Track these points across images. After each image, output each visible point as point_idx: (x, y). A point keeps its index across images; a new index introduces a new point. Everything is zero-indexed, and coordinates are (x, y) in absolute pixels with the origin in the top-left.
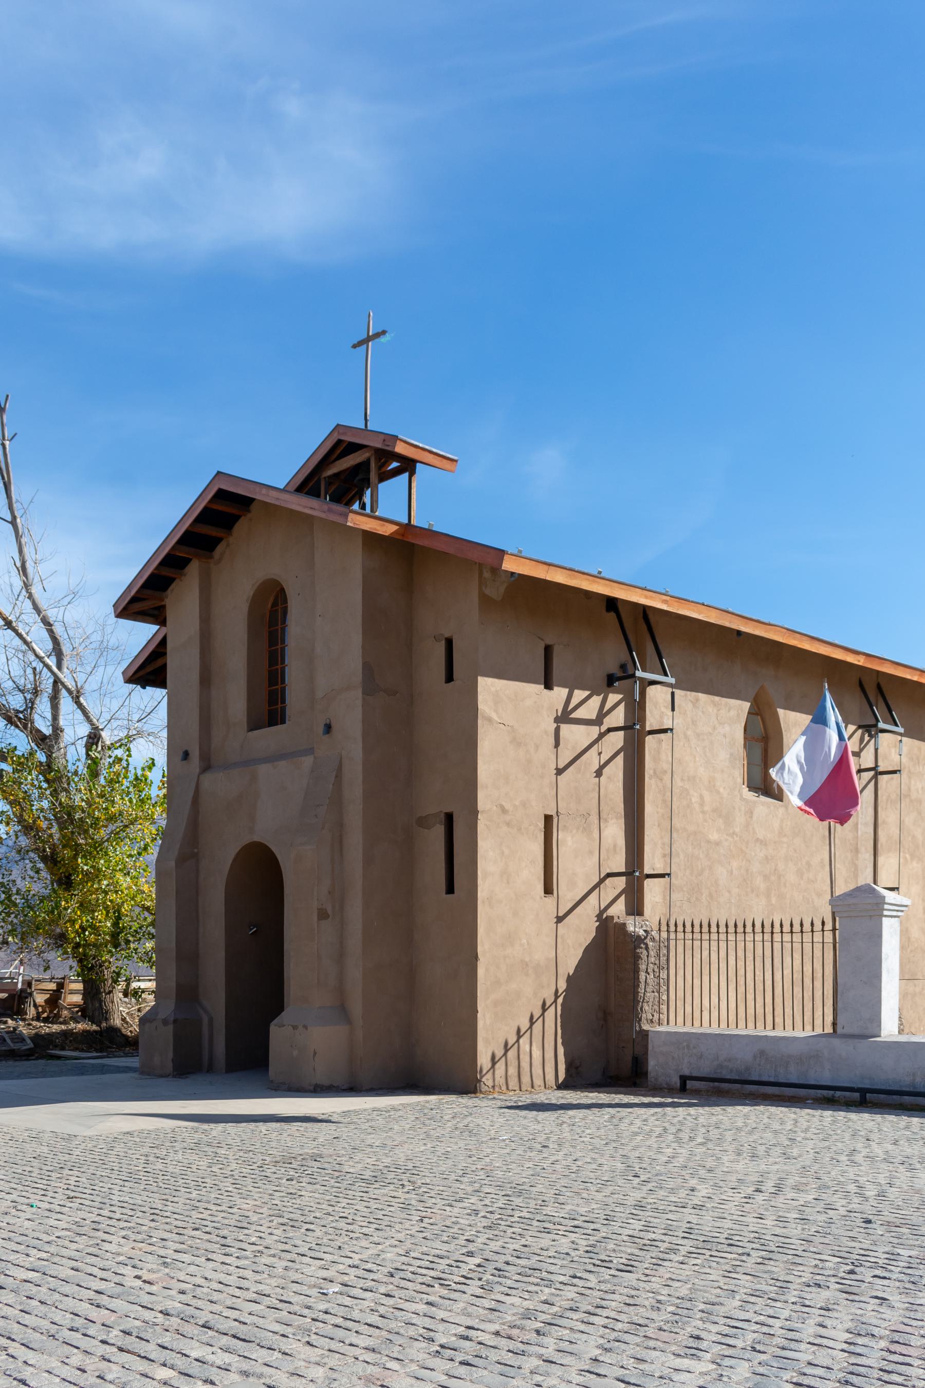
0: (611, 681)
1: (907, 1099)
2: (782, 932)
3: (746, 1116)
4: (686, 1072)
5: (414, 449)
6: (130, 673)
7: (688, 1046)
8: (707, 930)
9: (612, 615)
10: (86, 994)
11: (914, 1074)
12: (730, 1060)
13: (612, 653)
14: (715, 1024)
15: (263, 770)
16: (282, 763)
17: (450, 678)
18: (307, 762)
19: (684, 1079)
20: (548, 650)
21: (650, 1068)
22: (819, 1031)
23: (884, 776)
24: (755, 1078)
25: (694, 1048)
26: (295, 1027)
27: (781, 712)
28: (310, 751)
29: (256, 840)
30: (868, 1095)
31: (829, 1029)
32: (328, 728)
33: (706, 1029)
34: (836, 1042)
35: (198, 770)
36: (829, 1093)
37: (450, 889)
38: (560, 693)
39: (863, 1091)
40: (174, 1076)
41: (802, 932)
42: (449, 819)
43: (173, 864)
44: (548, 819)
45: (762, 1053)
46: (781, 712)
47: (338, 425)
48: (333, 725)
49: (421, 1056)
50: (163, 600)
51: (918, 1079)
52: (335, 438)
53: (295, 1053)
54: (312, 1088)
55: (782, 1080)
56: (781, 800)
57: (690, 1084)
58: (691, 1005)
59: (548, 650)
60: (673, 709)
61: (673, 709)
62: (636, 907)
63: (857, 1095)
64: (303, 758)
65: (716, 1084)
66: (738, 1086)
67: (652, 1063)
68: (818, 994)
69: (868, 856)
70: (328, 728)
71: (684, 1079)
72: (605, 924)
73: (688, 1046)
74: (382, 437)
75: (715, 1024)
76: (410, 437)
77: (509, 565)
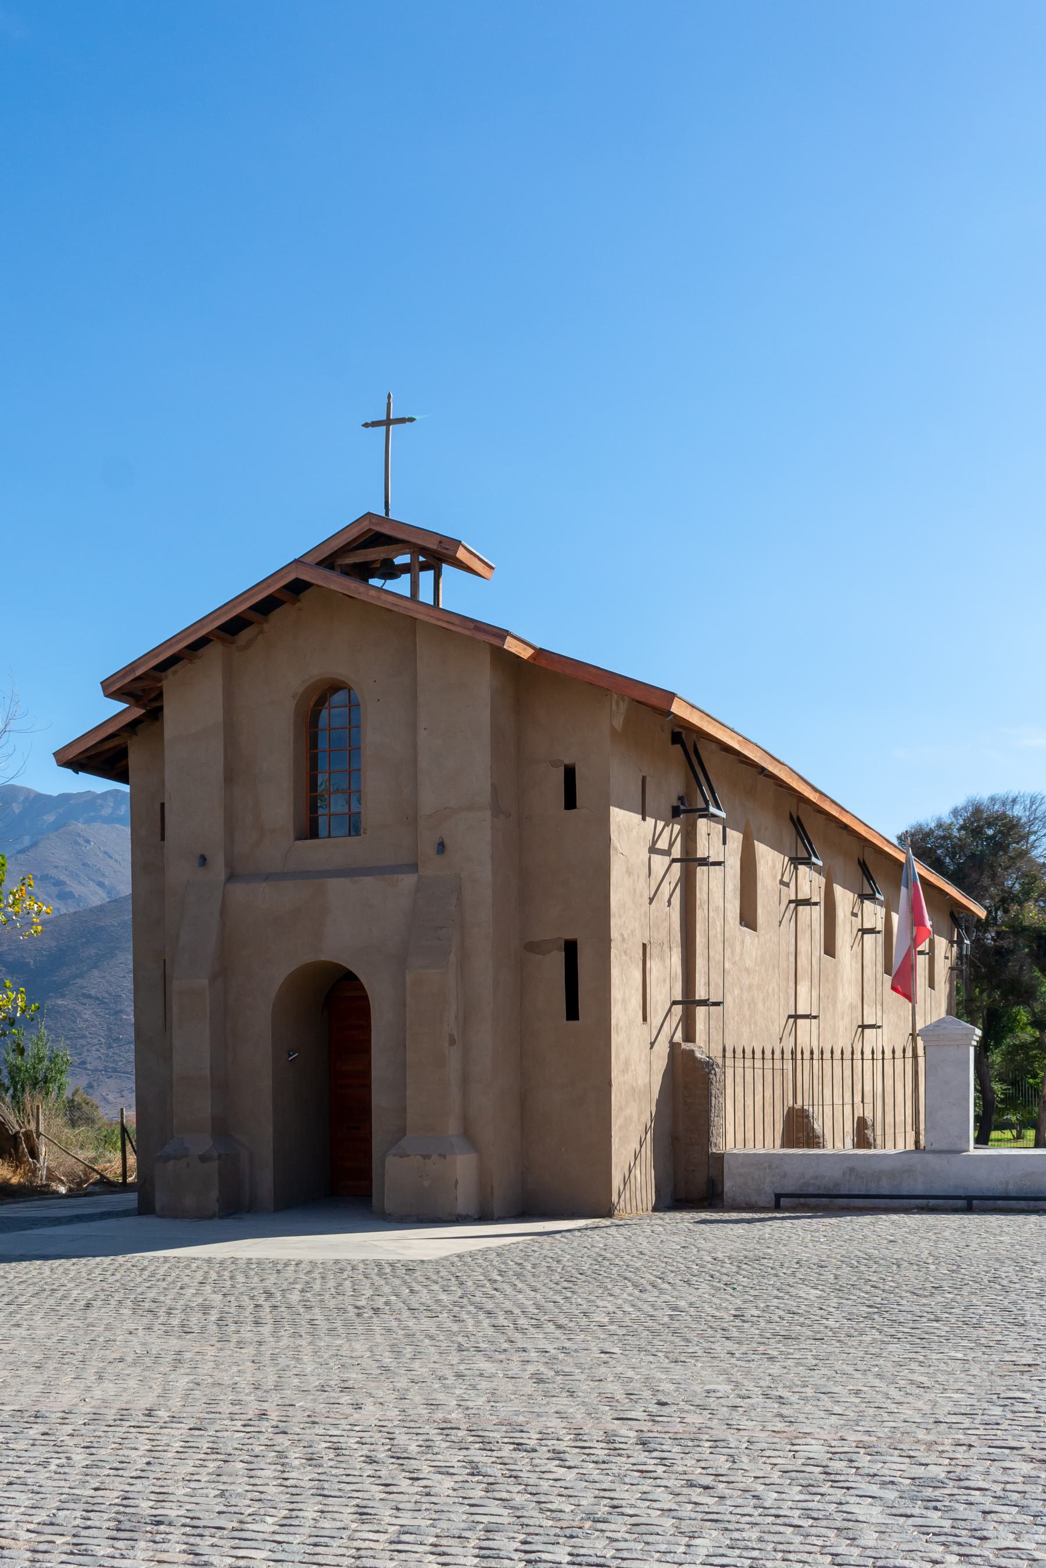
0: (676, 812)
2: (863, 1059)
3: (66, 1272)
4: (778, 1191)
5: (469, 555)
6: (71, 754)
7: (770, 1167)
8: (860, 1057)
9: (678, 747)
11: (1007, 1183)
12: (817, 1178)
13: (671, 784)
16: (368, 880)
17: (570, 803)
18: (408, 881)
19: (778, 1197)
21: (726, 1189)
22: (900, 1148)
25: (777, 1168)
26: (426, 1157)
27: (756, 842)
28: (414, 868)
30: (974, 1202)
32: (441, 847)
35: (222, 877)
36: (924, 1202)
37: (572, 1013)
39: (969, 1199)
40: (221, 1218)
41: (873, 1059)
44: (644, 945)
45: (852, 1170)
46: (756, 842)
47: (369, 513)
48: (447, 841)
49: (552, 1185)
50: (160, 681)
51: (1011, 1187)
52: (365, 526)
53: (426, 1184)
54: (454, 1218)
56: (755, 930)
58: (743, 1129)
60: (724, 843)
61: (724, 843)
62: (689, 1035)
63: (961, 1203)
65: (802, 1200)
67: (728, 1185)
71: (778, 1197)
73: (770, 1167)
74: (439, 539)
76: (473, 543)
77: (677, 708)
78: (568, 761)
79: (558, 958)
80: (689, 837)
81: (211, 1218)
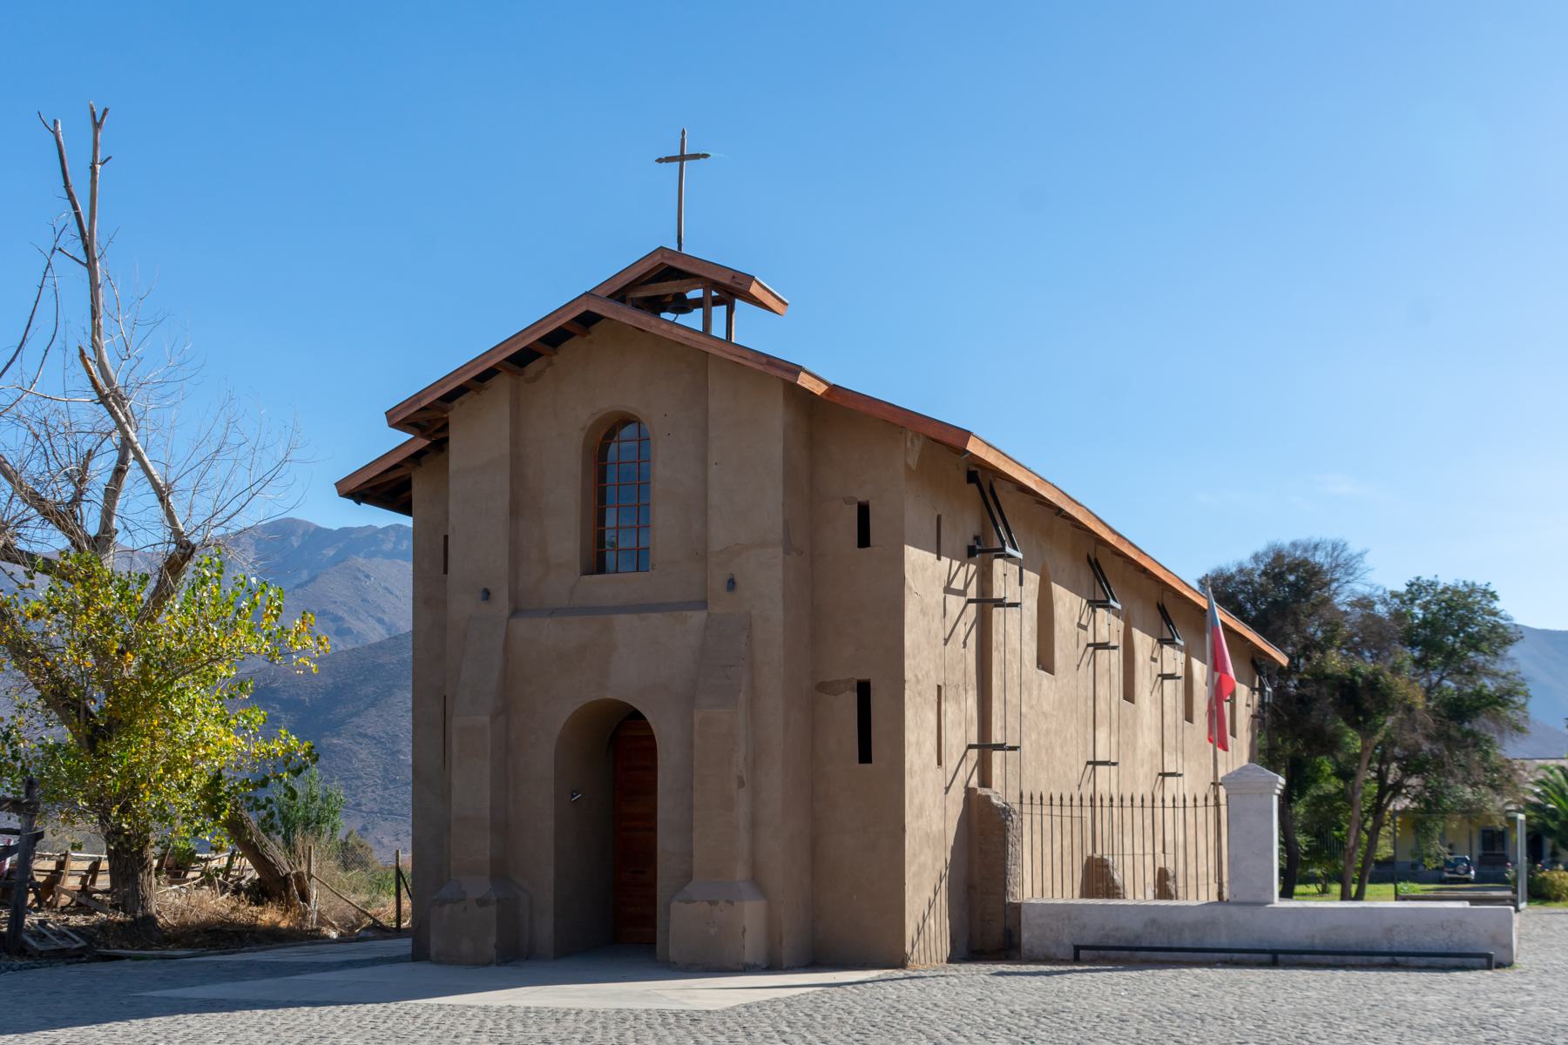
1: (1306, 958)
3: (1380, 982)
6: (353, 485)
9: (974, 486)
10: (257, 867)
14: (1057, 894)
15: (622, 621)
17: (864, 540)
18: (697, 618)
19: (1077, 949)
20: (939, 518)
23: (622, 616)
24: (1144, 944)
26: (712, 903)
28: (703, 604)
29: (609, 696)
31: (1216, 899)
32: (731, 584)
33: (1048, 900)
34: (1220, 908)
35: (506, 612)
37: (865, 756)
38: (945, 561)
42: (864, 689)
43: (486, 719)
45: (1153, 921)
48: (738, 579)
50: (446, 411)
52: (658, 259)
55: (1175, 945)
57: (1082, 953)
58: (1041, 878)
59: (939, 518)
60: (1021, 584)
61: (1021, 584)
62: (985, 781)
64: (689, 613)
66: (1126, 953)
67: (1025, 935)
68: (1047, 859)
69: (1090, 730)
70: (731, 584)
71: (1077, 949)
72: (969, 791)
75: (1057, 894)
76: (766, 280)
77: (973, 447)
78: (861, 499)
79: (851, 699)
80: (985, 577)
81: (488, 964)
